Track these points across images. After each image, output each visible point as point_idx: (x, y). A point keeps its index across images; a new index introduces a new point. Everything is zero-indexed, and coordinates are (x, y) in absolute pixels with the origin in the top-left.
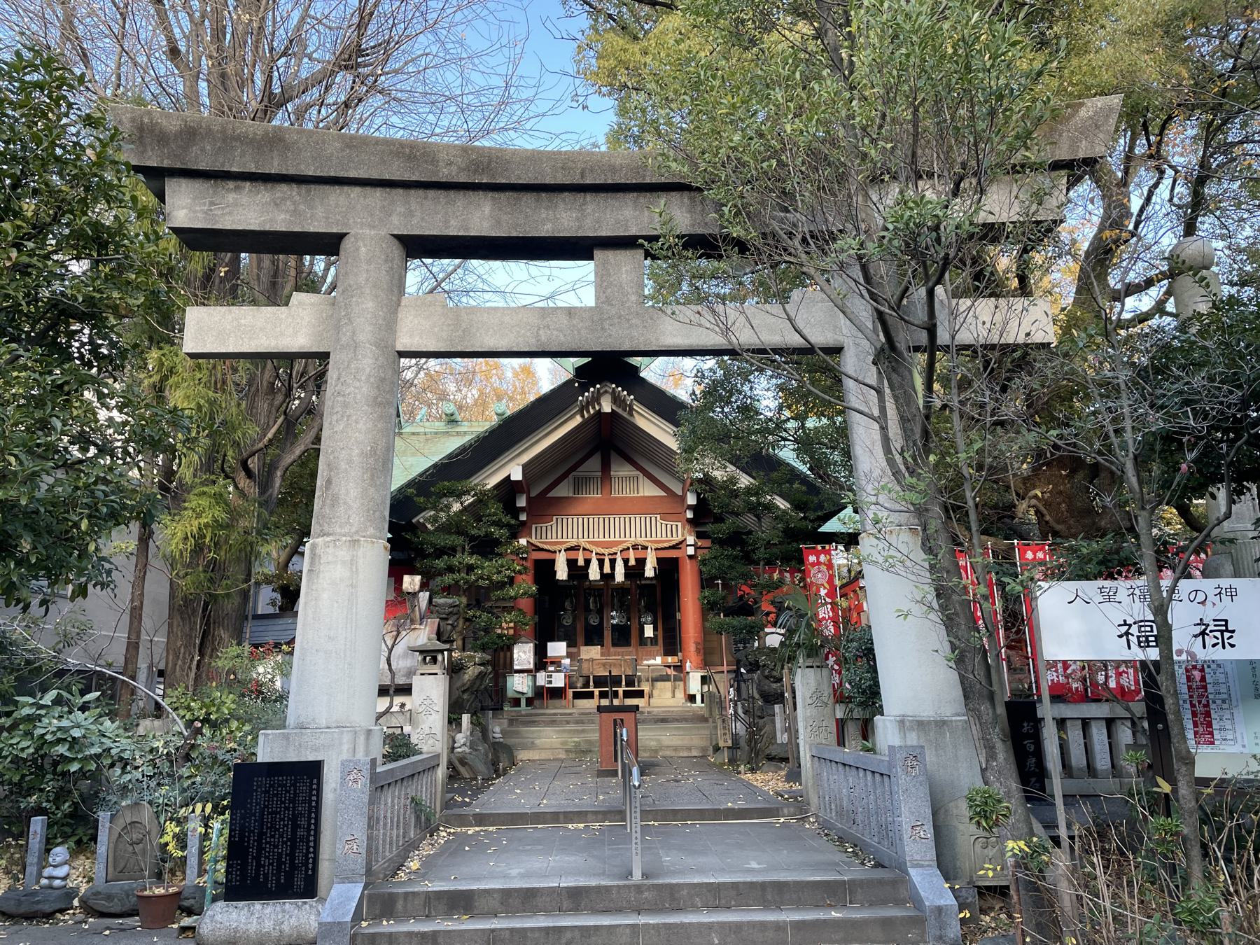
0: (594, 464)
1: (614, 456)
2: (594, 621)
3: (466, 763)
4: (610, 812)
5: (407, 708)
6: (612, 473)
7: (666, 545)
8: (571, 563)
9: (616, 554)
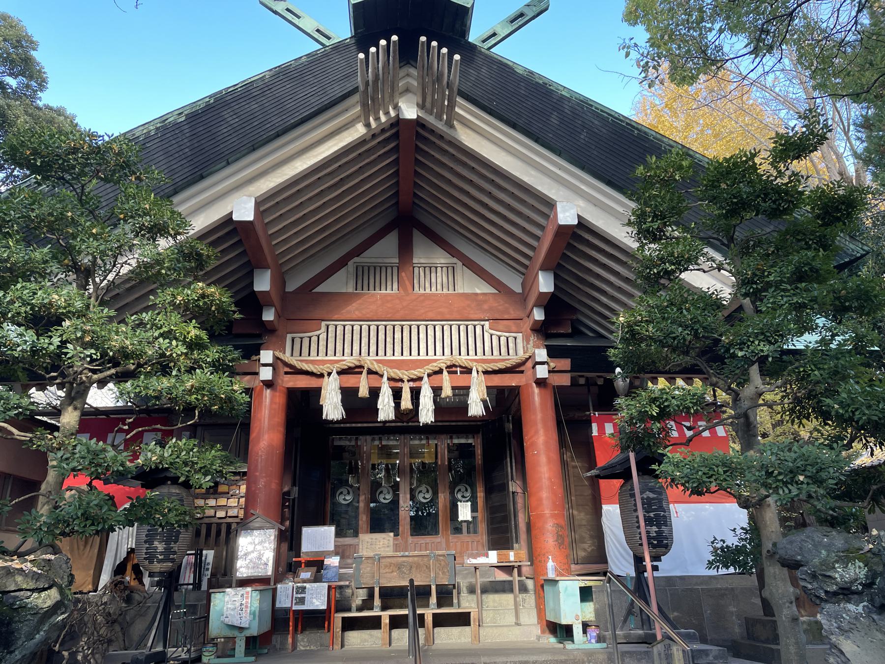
0: (390, 243)
1: (417, 237)
6: (414, 261)
8: (348, 395)
9: (420, 379)
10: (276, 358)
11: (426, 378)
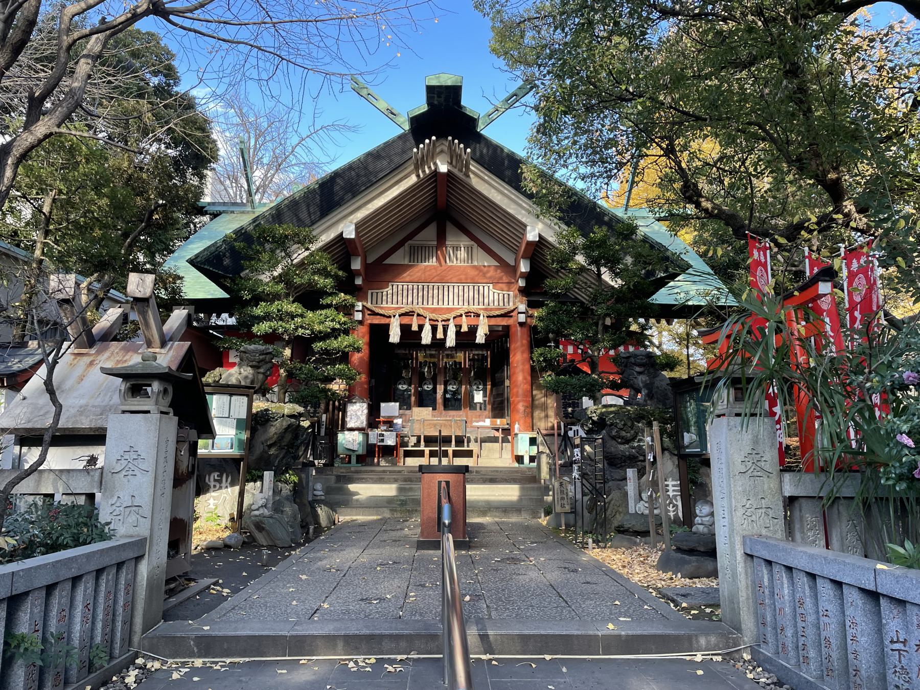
0: (430, 232)
1: (450, 227)
2: (428, 387)
3: (263, 529)
4: (419, 636)
5: (100, 463)
7: (498, 313)
8: (405, 329)
9: (449, 320)
10: (363, 306)
11: (452, 320)
